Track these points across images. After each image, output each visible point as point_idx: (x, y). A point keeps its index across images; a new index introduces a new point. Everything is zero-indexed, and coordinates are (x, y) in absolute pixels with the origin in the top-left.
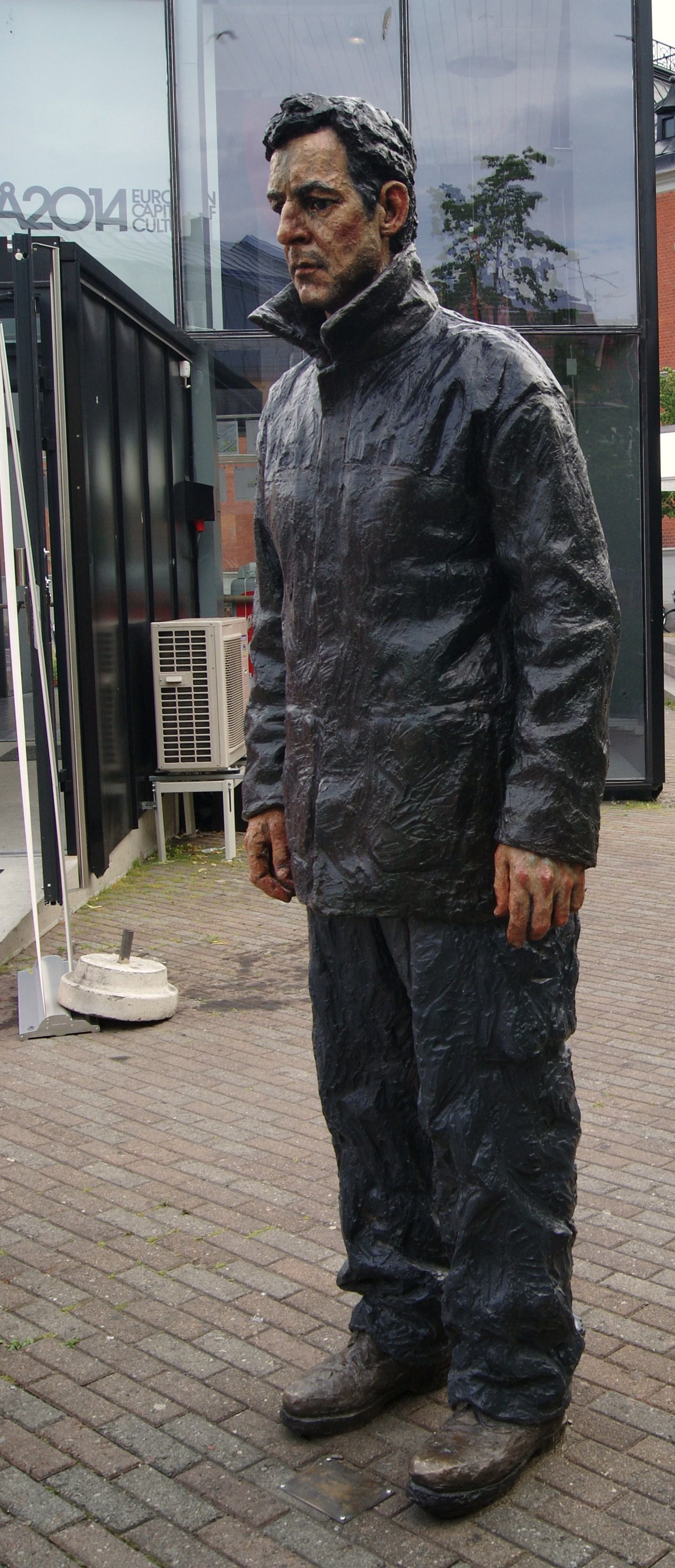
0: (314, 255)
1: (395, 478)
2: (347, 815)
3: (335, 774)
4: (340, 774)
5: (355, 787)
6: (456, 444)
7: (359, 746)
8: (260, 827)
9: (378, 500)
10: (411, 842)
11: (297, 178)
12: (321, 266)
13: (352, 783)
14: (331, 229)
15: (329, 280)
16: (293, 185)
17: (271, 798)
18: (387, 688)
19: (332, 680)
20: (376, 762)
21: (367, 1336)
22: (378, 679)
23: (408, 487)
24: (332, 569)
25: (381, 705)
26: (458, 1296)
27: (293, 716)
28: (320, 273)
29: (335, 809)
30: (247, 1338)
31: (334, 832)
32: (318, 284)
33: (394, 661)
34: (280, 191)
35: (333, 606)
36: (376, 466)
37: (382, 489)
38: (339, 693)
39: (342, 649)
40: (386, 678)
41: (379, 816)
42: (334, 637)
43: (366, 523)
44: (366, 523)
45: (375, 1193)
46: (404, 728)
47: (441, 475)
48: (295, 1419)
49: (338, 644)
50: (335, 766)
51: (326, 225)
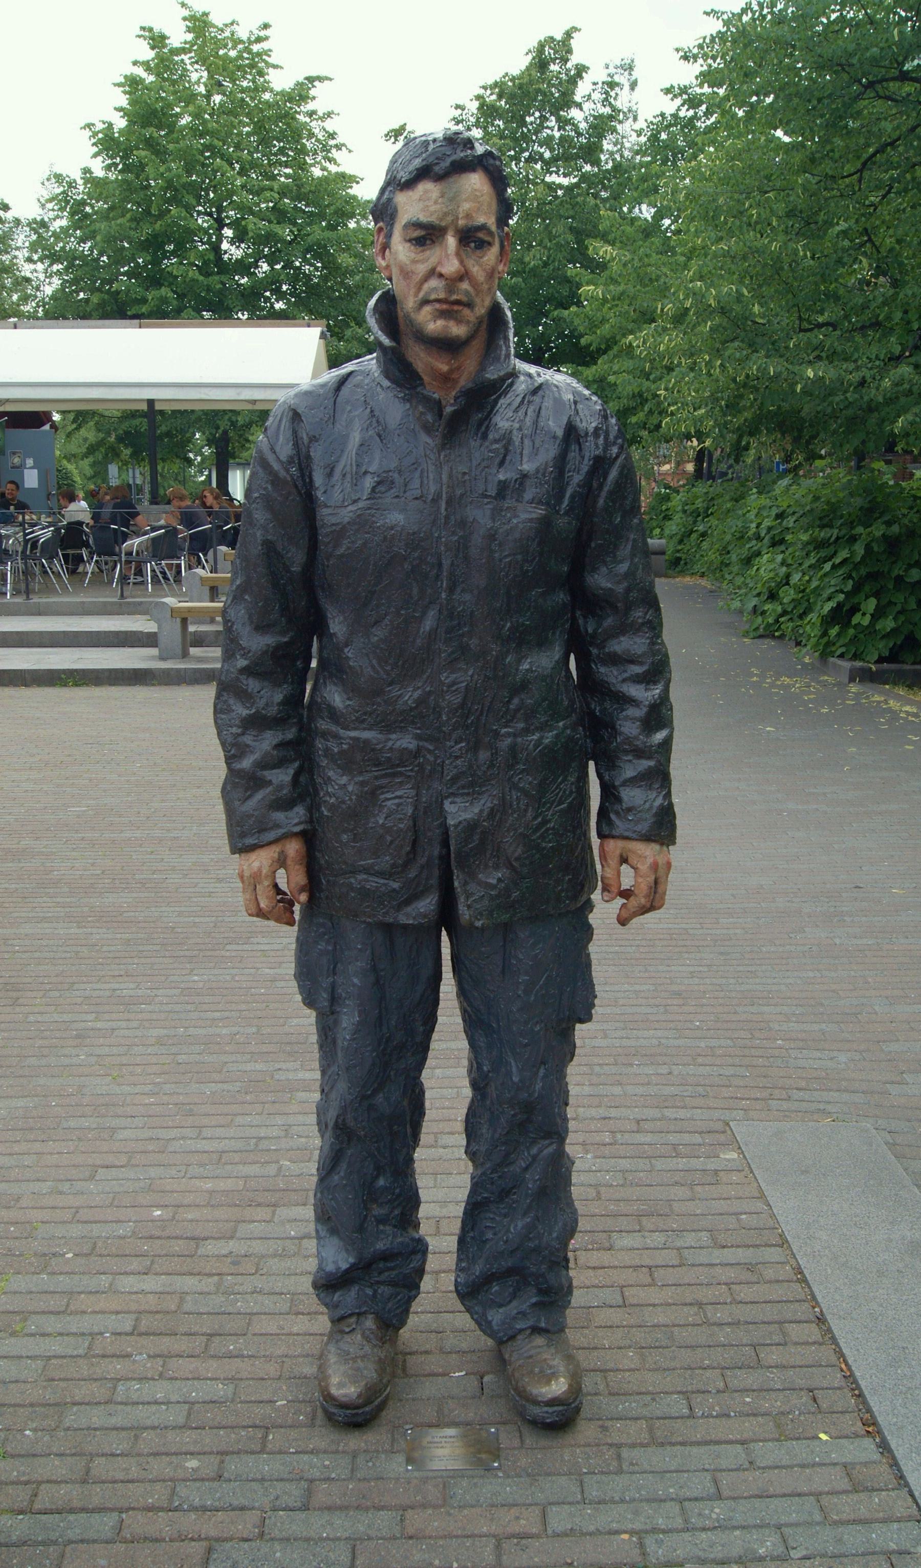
0: (467, 293)
1: (534, 516)
2: (482, 832)
3: (462, 795)
4: (468, 794)
5: (489, 805)
6: (578, 485)
7: (492, 766)
8: (276, 855)
9: (517, 535)
10: (544, 848)
11: (468, 216)
12: (469, 305)
13: (482, 802)
14: (484, 270)
15: (472, 319)
16: (461, 223)
17: (296, 825)
18: (517, 710)
19: (462, 705)
20: (509, 779)
21: (371, 1316)
22: (509, 702)
23: (545, 523)
24: (465, 599)
25: (510, 727)
26: (530, 1239)
27: (375, 741)
28: (466, 312)
29: (471, 827)
30: (161, 1375)
31: (471, 849)
32: (459, 321)
33: (523, 687)
34: (443, 224)
35: (463, 635)
36: (508, 503)
37: (521, 526)
38: (467, 717)
39: (472, 676)
40: (516, 701)
41: (516, 830)
42: (462, 665)
43: (506, 556)
44: (506, 556)
45: (381, 1182)
46: (536, 746)
47: (567, 513)
48: (360, 1411)
49: (466, 671)
50: (463, 787)
51: (481, 266)
